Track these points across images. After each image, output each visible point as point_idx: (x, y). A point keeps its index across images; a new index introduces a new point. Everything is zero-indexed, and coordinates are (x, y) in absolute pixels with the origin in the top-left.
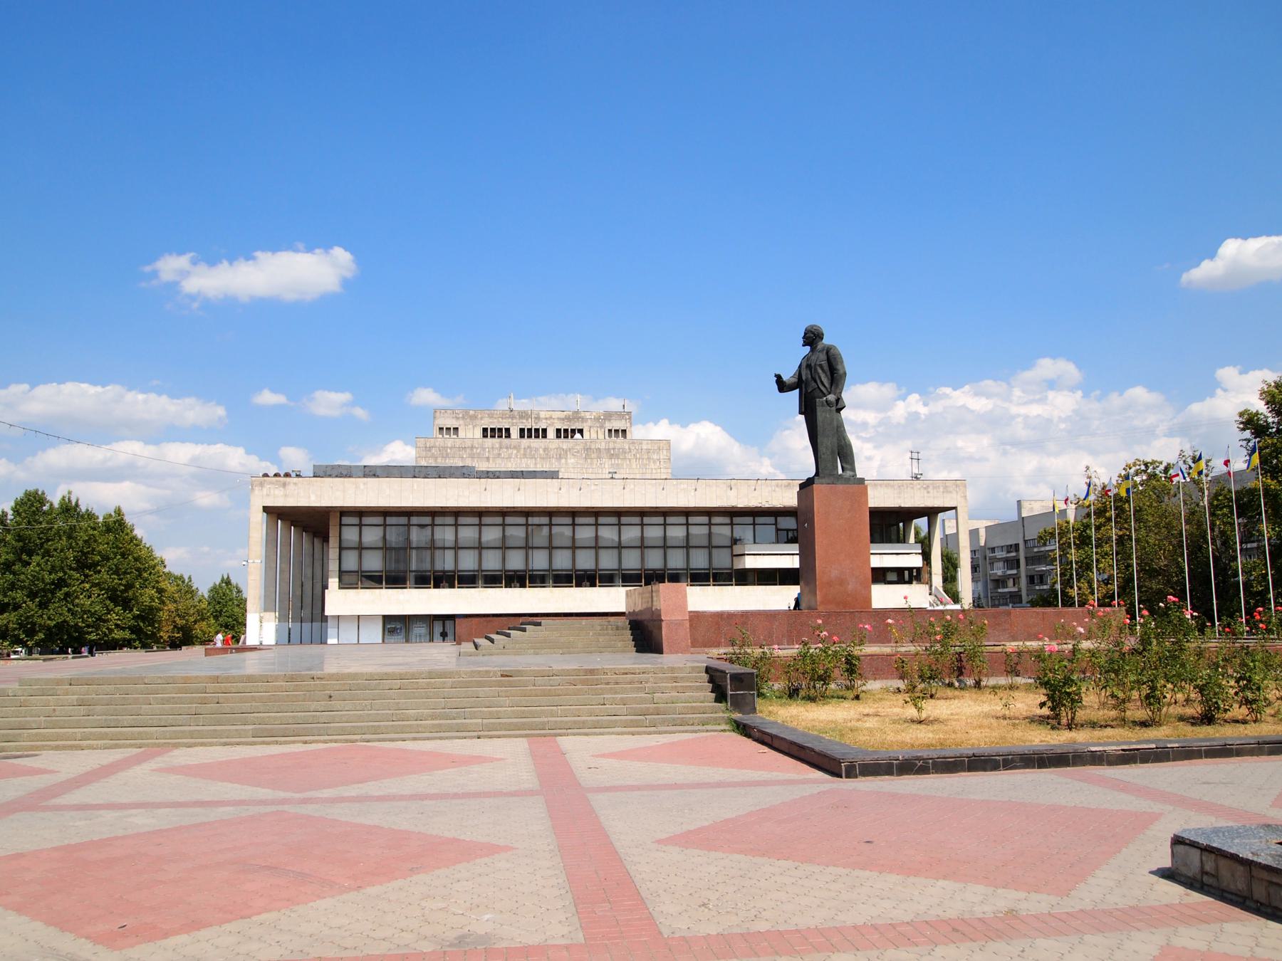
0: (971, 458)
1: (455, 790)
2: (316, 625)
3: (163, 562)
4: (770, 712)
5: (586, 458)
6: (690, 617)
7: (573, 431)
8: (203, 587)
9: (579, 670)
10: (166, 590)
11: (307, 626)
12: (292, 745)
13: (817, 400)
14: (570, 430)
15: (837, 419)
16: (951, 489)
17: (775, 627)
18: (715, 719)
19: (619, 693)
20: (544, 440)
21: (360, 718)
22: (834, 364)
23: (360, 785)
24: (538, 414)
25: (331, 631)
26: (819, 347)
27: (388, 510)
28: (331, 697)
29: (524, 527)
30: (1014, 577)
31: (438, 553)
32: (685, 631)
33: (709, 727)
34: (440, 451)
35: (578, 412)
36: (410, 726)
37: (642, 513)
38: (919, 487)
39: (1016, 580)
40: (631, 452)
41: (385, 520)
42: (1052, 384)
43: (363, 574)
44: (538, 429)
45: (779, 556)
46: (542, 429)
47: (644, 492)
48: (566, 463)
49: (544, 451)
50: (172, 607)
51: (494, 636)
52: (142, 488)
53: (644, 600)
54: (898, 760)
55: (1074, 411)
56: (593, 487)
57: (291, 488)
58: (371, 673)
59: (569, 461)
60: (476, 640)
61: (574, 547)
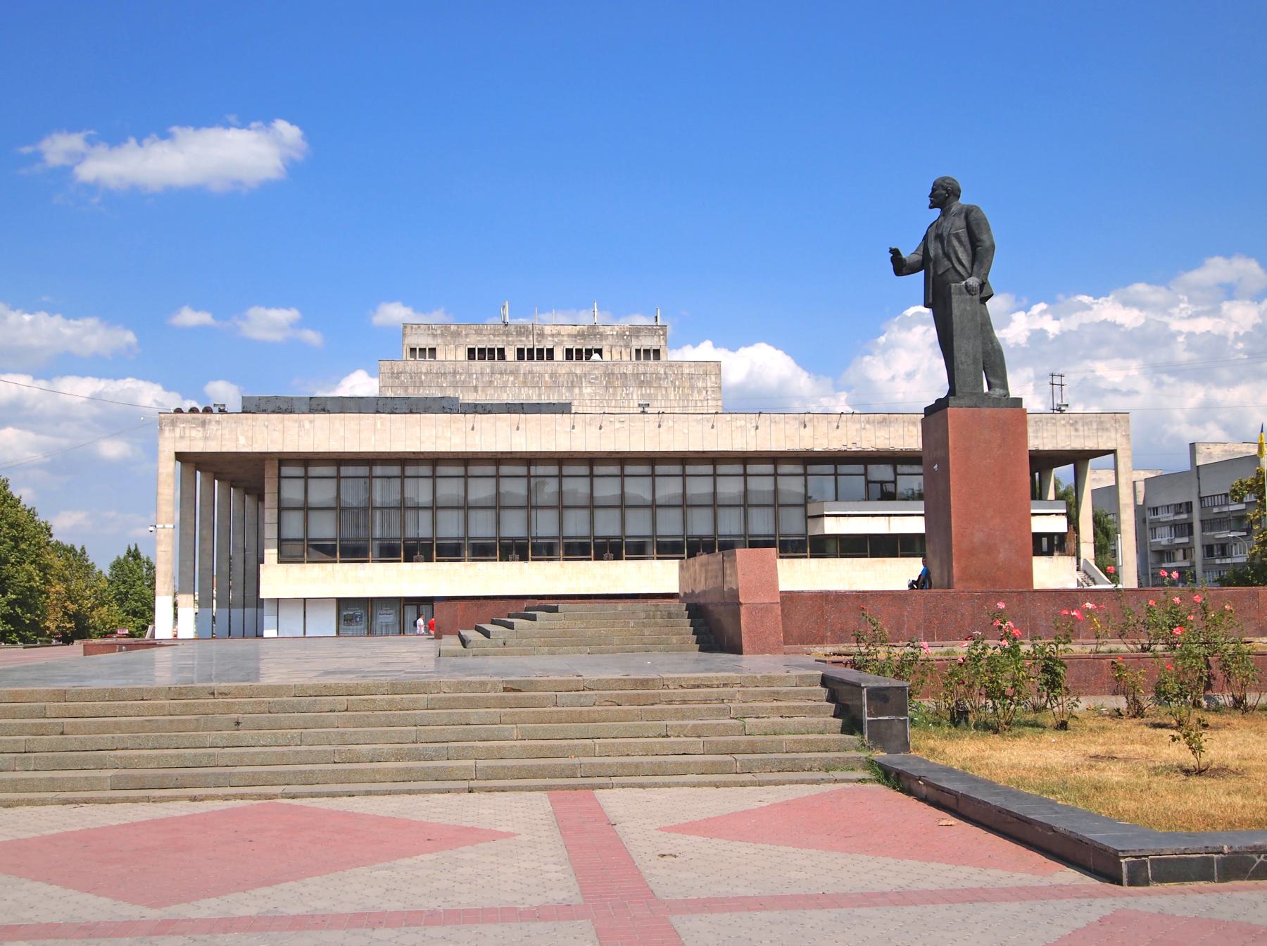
0: (1115, 391)
1: (433, 904)
2: (250, 611)
3: (48, 529)
4: (932, 750)
5: (607, 387)
6: (782, 598)
7: (589, 352)
8: (102, 563)
9: (625, 680)
10: (52, 567)
11: (237, 613)
12: (172, 804)
13: (953, 285)
14: (584, 351)
15: (982, 313)
16: (1108, 426)
17: (906, 613)
18: (847, 760)
19: (688, 718)
20: (550, 363)
21: (282, 759)
22: (977, 232)
23: (267, 891)
24: (542, 330)
25: (269, 620)
26: (954, 209)
27: (343, 457)
28: (238, 723)
29: (525, 480)
30: (1186, 546)
31: (410, 515)
32: (775, 619)
33: (838, 774)
34: (411, 378)
35: (594, 326)
36: (362, 771)
37: (684, 459)
38: (1063, 422)
39: (1188, 552)
40: (667, 378)
41: (339, 471)
42: (1229, 291)
43: (310, 543)
44: (543, 350)
45: (870, 518)
46: (547, 349)
47: (686, 431)
48: (581, 394)
49: (551, 378)
50: (60, 587)
51: (488, 627)
52: (30, 436)
53: (709, 574)
54: (1222, 853)
55: (1255, 326)
56: (618, 425)
57: (213, 428)
58: (302, 686)
59: (585, 391)
60: (463, 632)
61: (592, 506)
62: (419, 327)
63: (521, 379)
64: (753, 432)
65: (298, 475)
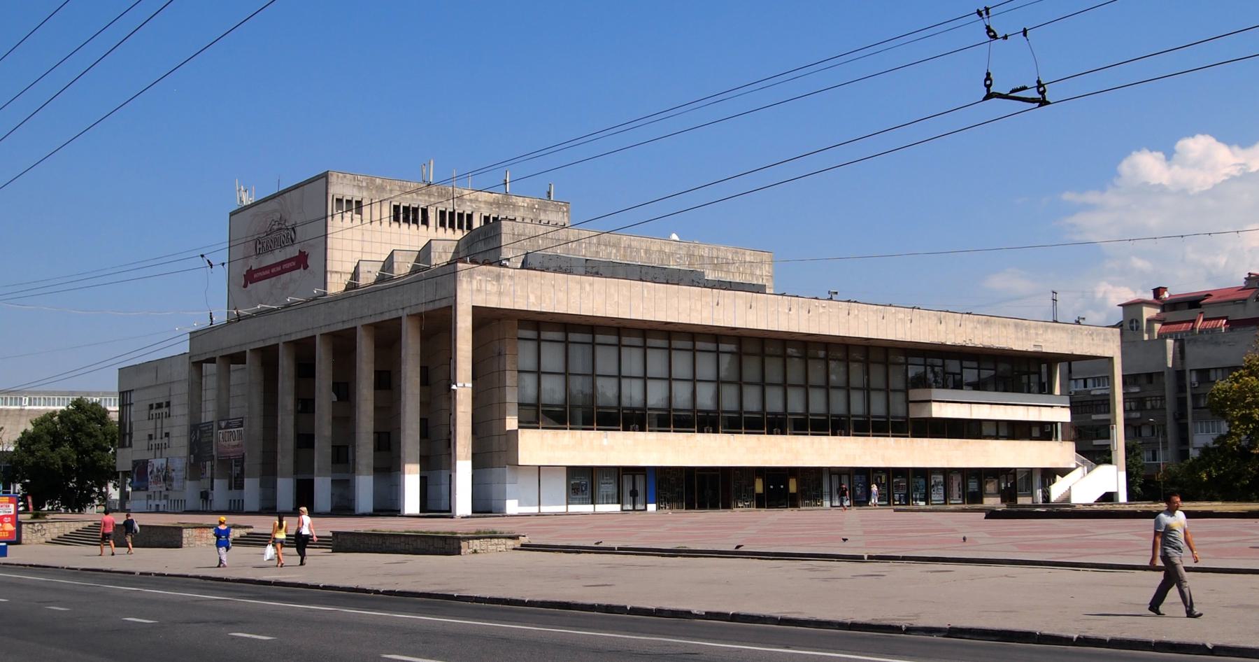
45: (959, 404)
47: (866, 319)
49: (646, 253)
56: (821, 310)
62: (345, 177)
63: (622, 252)
64: (909, 325)
65: (661, 346)
